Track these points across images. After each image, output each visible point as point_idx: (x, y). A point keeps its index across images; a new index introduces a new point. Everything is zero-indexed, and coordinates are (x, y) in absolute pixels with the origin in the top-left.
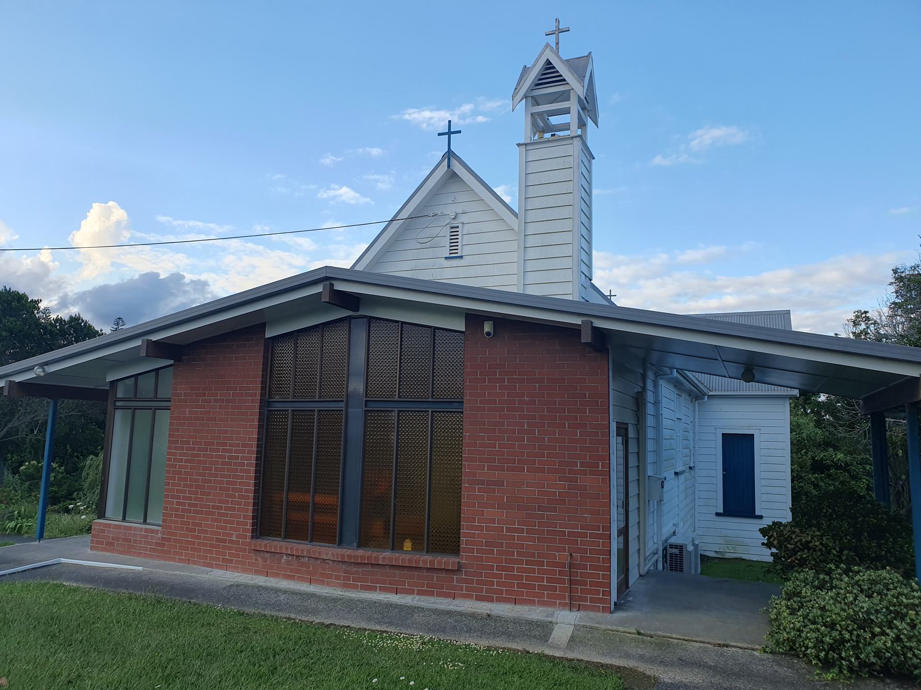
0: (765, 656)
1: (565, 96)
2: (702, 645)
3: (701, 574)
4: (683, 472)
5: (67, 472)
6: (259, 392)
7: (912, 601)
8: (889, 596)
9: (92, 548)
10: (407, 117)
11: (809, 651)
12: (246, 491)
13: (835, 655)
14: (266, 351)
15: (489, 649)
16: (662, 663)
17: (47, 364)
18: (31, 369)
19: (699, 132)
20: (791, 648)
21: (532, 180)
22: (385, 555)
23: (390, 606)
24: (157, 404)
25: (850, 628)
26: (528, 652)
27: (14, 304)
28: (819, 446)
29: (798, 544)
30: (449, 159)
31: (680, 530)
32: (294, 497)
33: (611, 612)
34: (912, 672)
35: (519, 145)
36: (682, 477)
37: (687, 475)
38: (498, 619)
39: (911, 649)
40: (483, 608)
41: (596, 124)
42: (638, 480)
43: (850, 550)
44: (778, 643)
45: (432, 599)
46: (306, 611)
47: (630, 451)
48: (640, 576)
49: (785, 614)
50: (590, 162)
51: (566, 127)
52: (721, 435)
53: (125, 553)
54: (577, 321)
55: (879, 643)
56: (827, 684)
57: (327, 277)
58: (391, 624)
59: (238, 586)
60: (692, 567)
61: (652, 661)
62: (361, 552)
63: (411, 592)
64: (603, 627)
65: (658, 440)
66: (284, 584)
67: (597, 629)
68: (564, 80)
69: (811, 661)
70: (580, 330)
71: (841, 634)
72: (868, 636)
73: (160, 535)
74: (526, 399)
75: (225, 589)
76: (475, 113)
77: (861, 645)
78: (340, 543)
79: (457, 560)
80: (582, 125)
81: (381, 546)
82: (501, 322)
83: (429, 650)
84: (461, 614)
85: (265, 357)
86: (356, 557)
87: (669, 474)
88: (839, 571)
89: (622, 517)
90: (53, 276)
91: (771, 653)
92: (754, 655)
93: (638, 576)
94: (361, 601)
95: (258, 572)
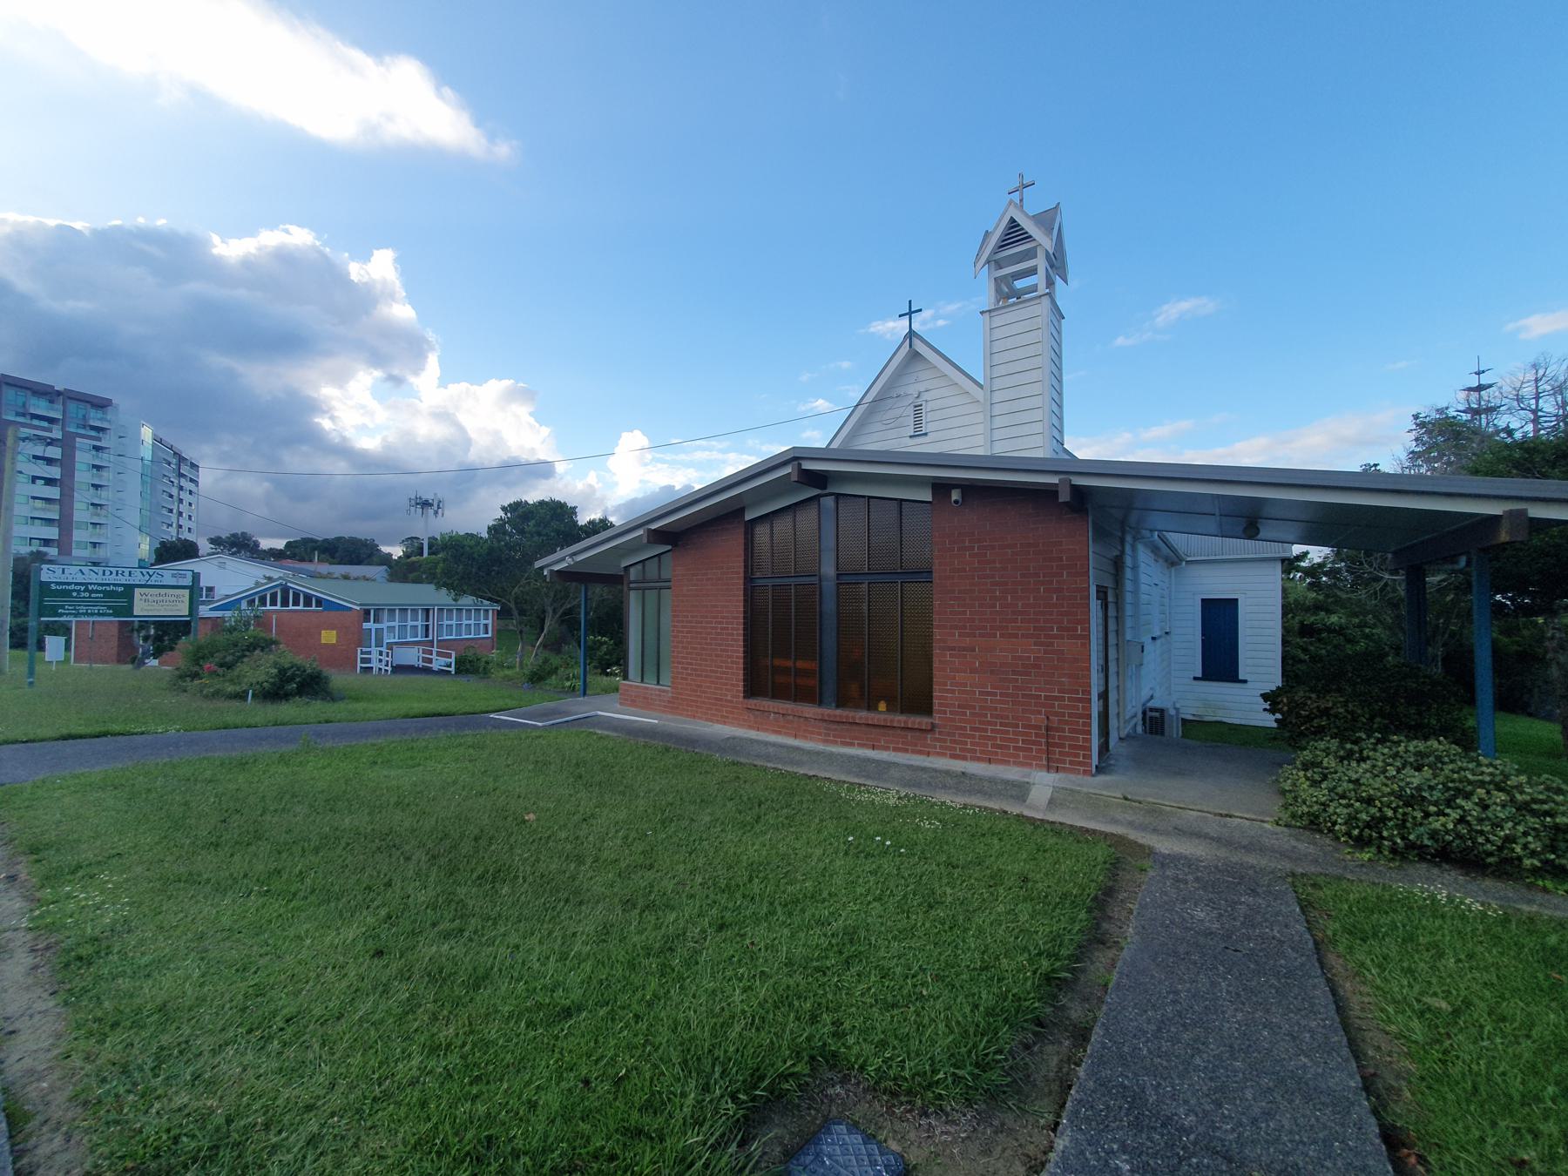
0: (1279, 829)
1: (1031, 254)
2: (1199, 813)
3: (1182, 737)
4: (1160, 637)
5: (615, 644)
6: (742, 570)
7: (1480, 777)
8: (1447, 772)
9: (621, 704)
10: (872, 330)
11: (1337, 828)
12: (737, 657)
13: (1374, 834)
14: (746, 533)
15: (965, 807)
16: (1155, 830)
17: (575, 554)
18: (563, 559)
19: (1165, 307)
20: (1312, 822)
21: (998, 346)
22: (862, 715)
23: (868, 760)
24: (661, 585)
25: (1394, 805)
26: (1006, 812)
27: (559, 511)
28: (1307, 610)
29: (1315, 711)
30: (911, 339)
31: (1157, 695)
32: (777, 662)
33: (1093, 776)
34: (1483, 860)
35: (982, 313)
36: (1158, 642)
37: (1163, 640)
38: (972, 777)
39: (1481, 833)
40: (958, 766)
41: (1066, 282)
42: (1117, 645)
43: (1383, 717)
44: (1293, 816)
45: (908, 756)
46: (792, 763)
47: (1109, 614)
48: (1120, 739)
49: (1305, 786)
50: (1059, 321)
51: (1034, 288)
52: (1199, 603)
53: (642, 708)
54: (1054, 480)
55: (1436, 823)
56: (1362, 865)
57: (795, 458)
58: (868, 777)
59: (734, 738)
60: (1174, 730)
61: (1142, 828)
62: (839, 712)
63: (887, 748)
64: (1085, 790)
65: (1136, 604)
66: (773, 738)
67: (1079, 792)
68: (1030, 237)
69: (1338, 839)
70: (1057, 492)
71: (1380, 810)
72: (1419, 815)
73: (670, 695)
74: (998, 565)
75: (722, 740)
76: (935, 318)
77: (1409, 825)
78: (821, 703)
79: (930, 720)
80: (1050, 283)
81: (857, 707)
82: (972, 490)
83: (906, 806)
84: (935, 770)
85: (746, 538)
86: (835, 716)
87: (1146, 639)
88: (1372, 740)
89: (1102, 682)
90: (598, 495)
91: (1286, 826)
92: (1264, 828)
93: (1117, 739)
94: (842, 756)
95: (750, 727)
